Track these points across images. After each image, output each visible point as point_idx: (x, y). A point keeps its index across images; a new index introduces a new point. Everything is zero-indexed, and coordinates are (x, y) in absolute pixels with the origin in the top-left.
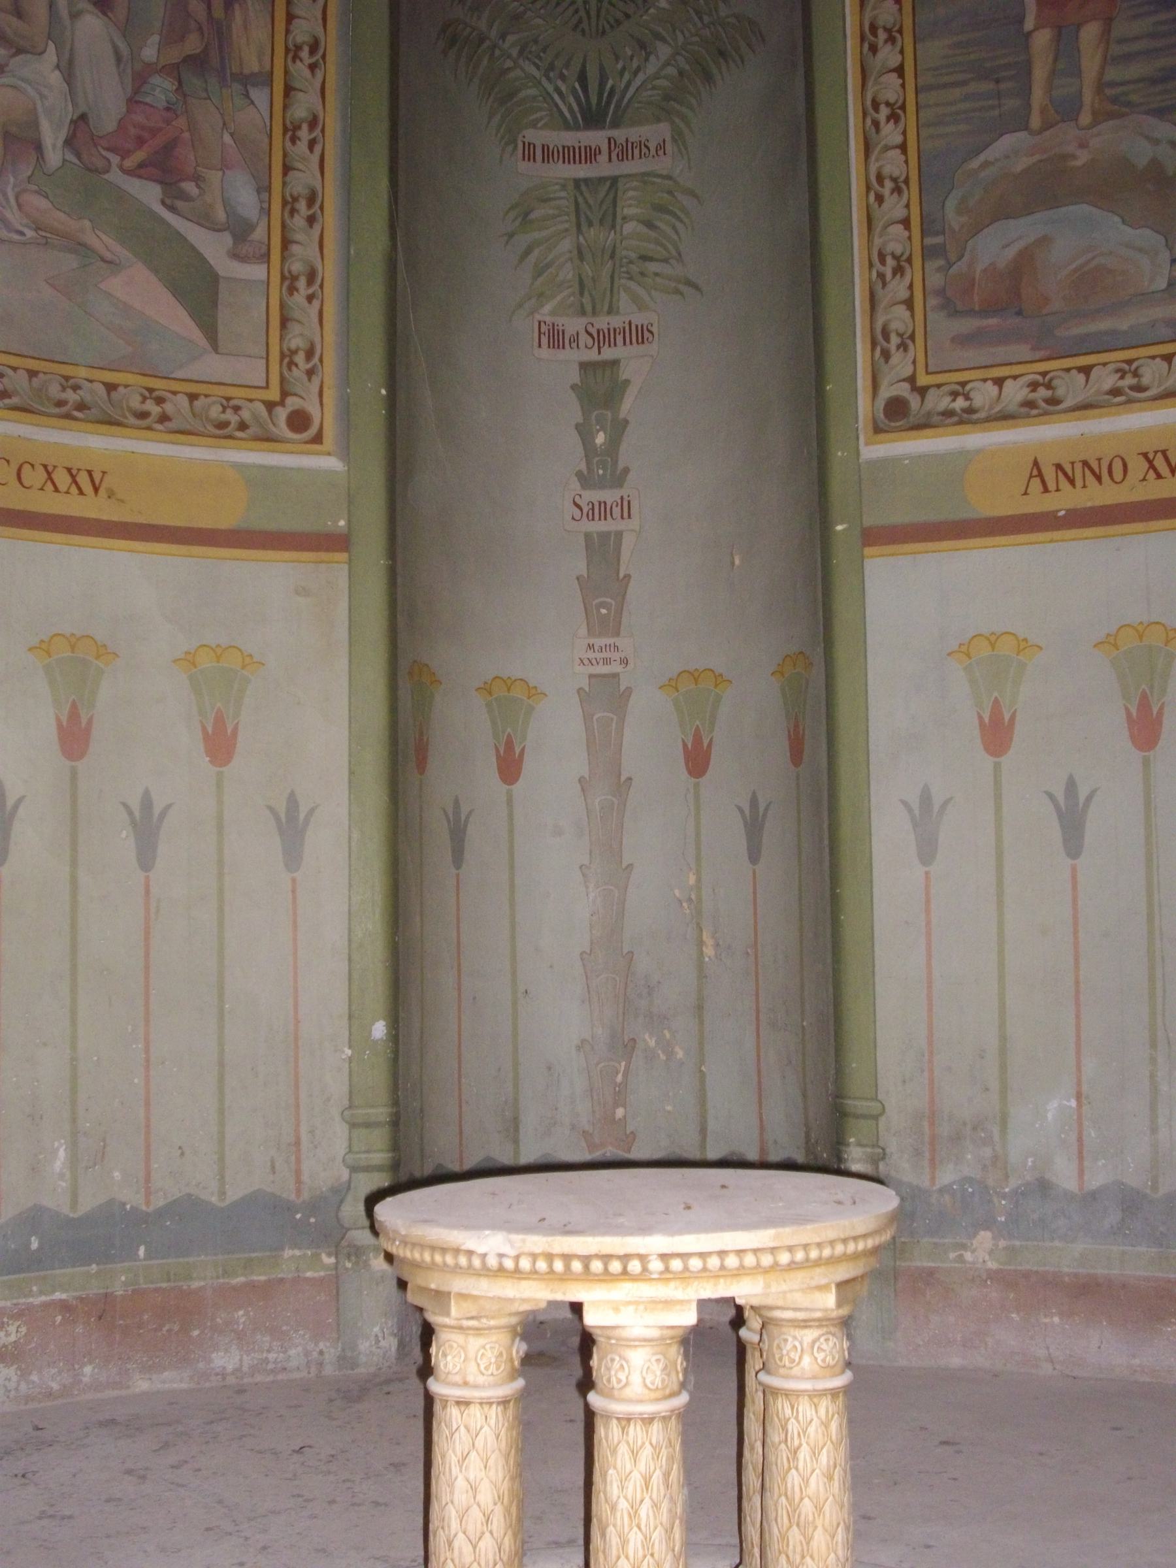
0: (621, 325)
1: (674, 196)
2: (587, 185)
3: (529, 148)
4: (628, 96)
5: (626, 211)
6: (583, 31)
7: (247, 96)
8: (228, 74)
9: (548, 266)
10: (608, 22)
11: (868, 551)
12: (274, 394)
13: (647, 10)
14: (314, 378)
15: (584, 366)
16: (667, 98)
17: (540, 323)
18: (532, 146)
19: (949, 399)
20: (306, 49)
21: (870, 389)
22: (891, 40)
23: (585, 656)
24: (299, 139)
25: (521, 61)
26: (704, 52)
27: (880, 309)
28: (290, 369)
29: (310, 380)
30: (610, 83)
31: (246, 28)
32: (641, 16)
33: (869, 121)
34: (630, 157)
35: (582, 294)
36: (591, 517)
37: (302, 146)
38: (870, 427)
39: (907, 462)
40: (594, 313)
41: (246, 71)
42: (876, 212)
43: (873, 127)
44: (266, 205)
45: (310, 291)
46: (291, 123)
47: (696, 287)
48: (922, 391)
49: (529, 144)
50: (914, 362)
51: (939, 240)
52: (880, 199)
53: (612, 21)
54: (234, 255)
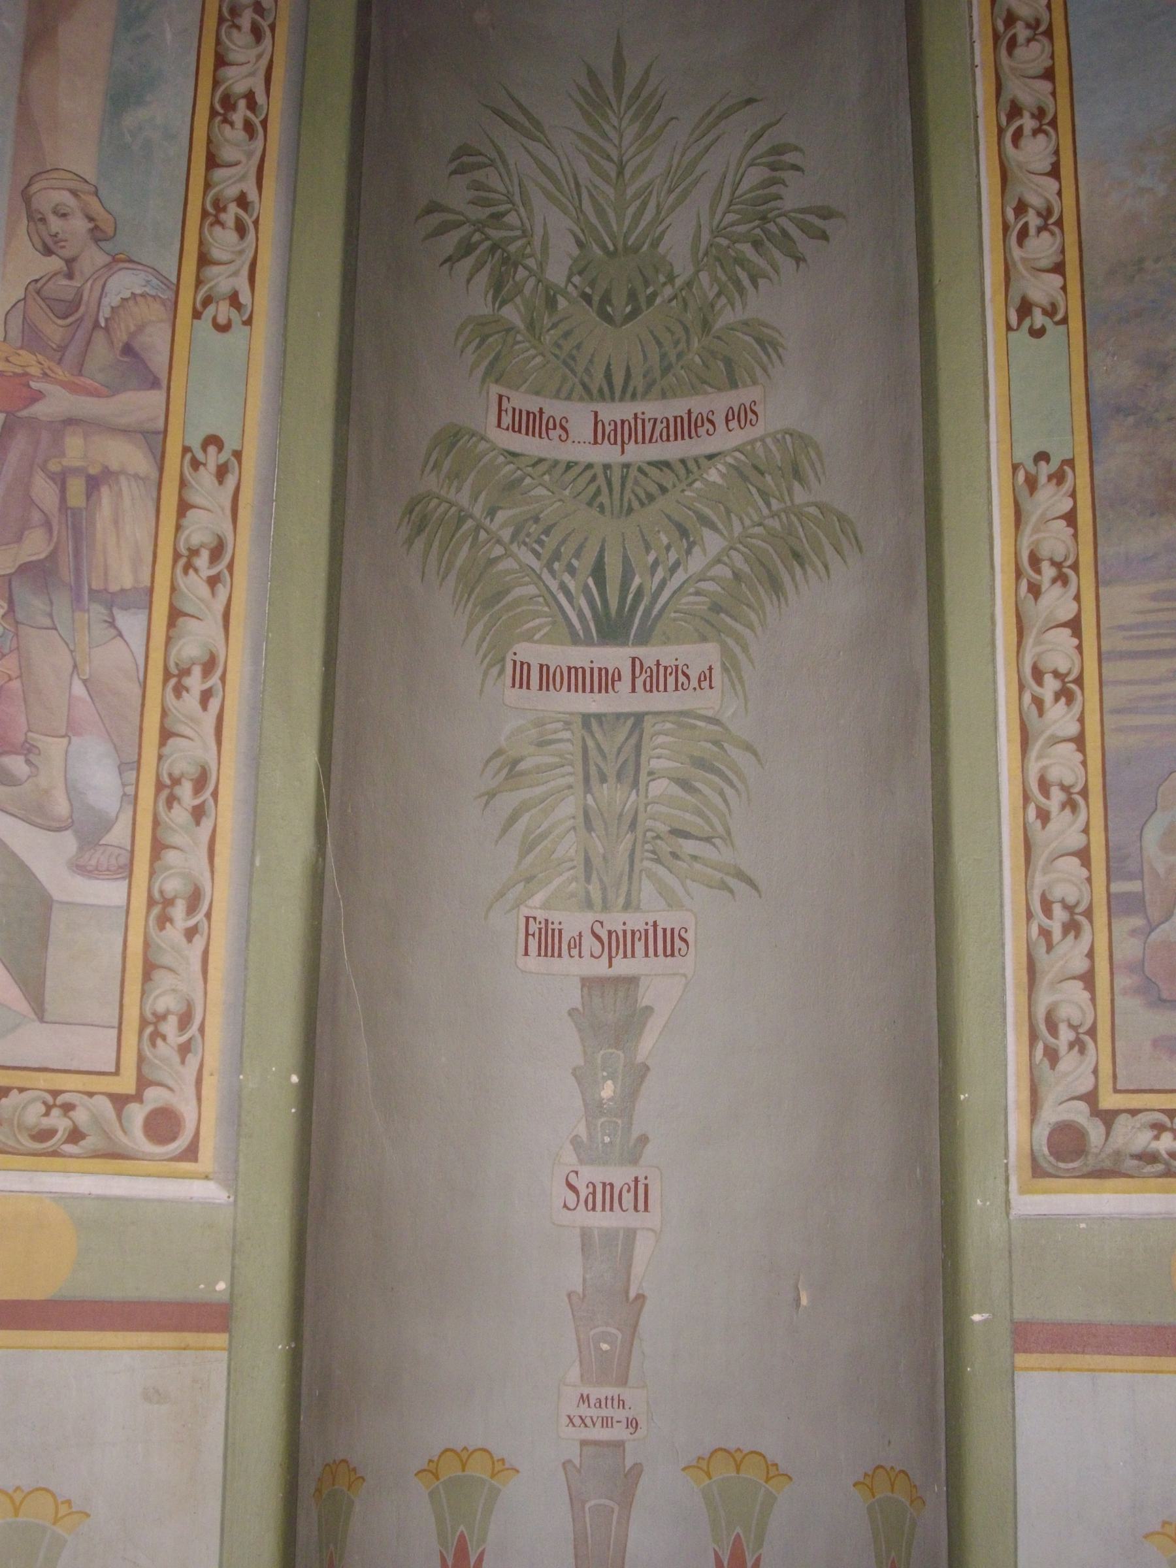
0: (642, 928)
1: (722, 748)
2: (601, 724)
3: (522, 668)
4: (662, 600)
5: (654, 764)
6: (602, 507)
7: (112, 624)
8: (86, 591)
9: (543, 837)
10: (636, 495)
11: (1021, 1359)
12: (126, 1084)
13: (690, 485)
14: (197, 938)
15: (587, 983)
16: (716, 608)
17: (527, 918)
18: (525, 667)
19: (1149, 1134)
20: (205, 555)
21: (1027, 1109)
22: (1061, 579)
23: (574, 1412)
24: (187, 691)
25: (514, 547)
26: (771, 550)
27: (1044, 983)
28: (154, 1044)
29: (183, 1062)
30: (637, 581)
31: (116, 522)
32: (683, 491)
33: (1027, 698)
34: (661, 687)
35: (588, 879)
36: (590, 1206)
37: (191, 701)
38: (1027, 1163)
39: (1083, 1226)
40: (606, 907)
41: (114, 587)
42: (1039, 835)
43: (1034, 707)
44: (130, 790)
45: (191, 923)
46: (177, 665)
47: (751, 883)
48: (1108, 1118)
49: (522, 664)
50: (1095, 1072)
51: (1134, 886)
52: (1044, 816)
53: (643, 496)
54: (77, 866)
